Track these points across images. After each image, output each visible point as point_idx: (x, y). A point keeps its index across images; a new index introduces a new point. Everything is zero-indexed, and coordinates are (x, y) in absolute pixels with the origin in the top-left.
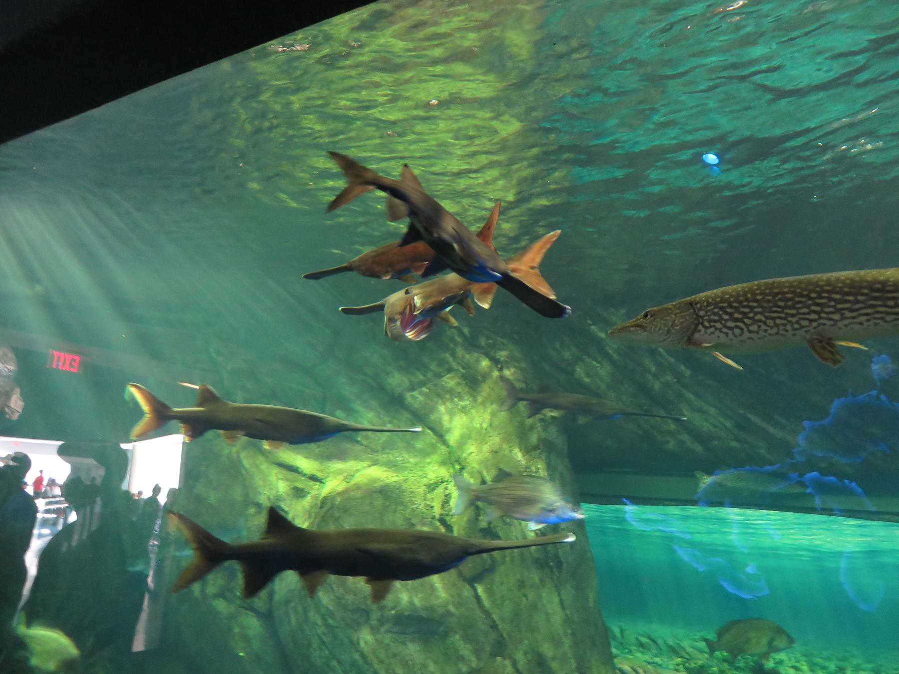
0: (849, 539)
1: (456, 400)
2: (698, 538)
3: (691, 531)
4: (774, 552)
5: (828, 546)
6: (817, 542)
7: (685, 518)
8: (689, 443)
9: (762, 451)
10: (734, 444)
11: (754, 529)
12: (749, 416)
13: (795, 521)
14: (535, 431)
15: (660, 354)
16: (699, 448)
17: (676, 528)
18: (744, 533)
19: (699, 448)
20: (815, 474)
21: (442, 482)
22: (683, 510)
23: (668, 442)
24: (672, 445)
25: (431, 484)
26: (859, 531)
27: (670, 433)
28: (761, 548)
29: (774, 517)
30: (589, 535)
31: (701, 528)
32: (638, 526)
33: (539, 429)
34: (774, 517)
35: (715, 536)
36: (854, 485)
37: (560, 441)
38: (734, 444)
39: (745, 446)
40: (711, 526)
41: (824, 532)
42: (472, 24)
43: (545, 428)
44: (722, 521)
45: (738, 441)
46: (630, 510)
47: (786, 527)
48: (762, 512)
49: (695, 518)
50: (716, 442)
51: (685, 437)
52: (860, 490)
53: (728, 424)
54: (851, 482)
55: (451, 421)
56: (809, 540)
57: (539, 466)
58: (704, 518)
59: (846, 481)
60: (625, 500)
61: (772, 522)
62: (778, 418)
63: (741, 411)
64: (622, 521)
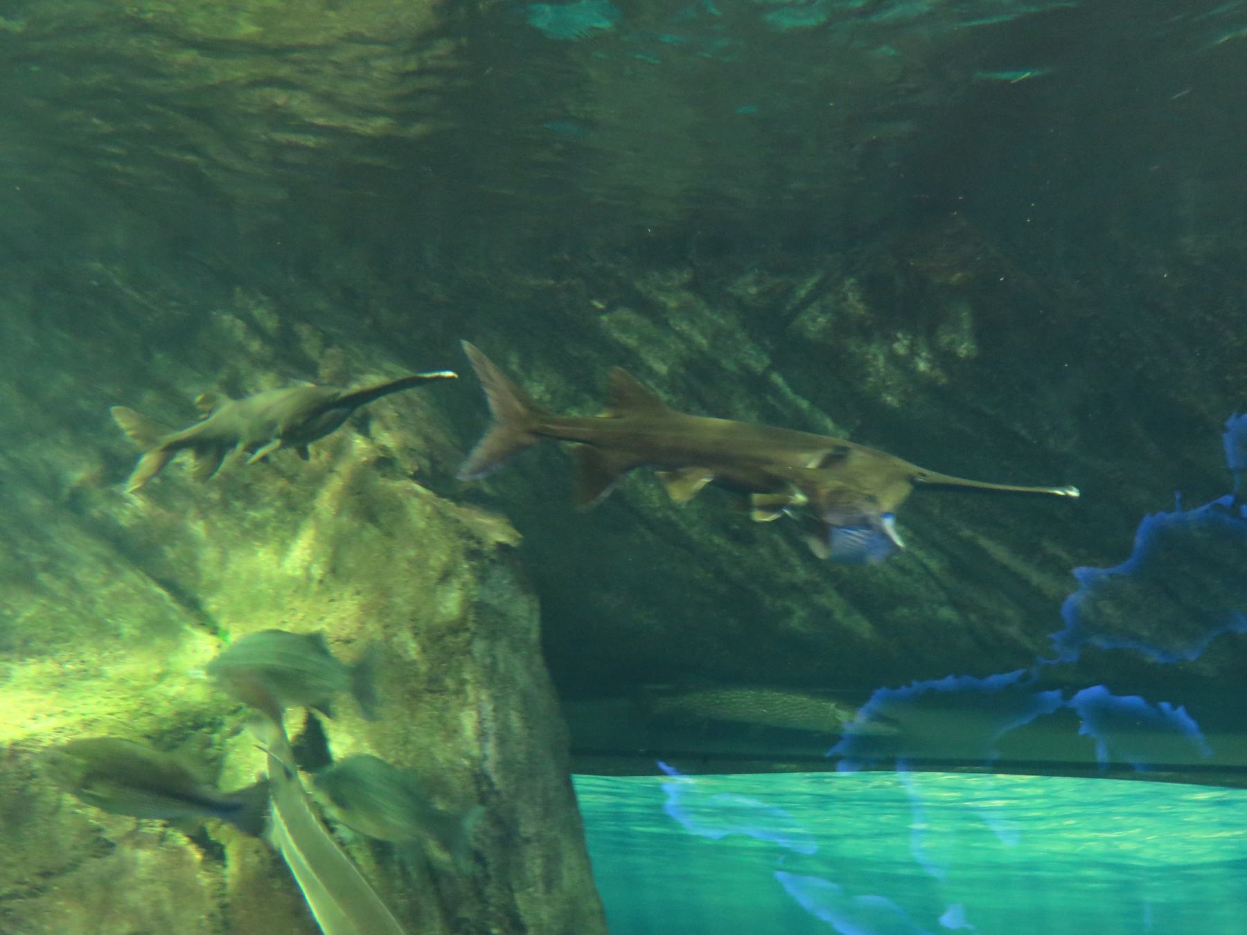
0: (1196, 835)
1: (238, 505)
2: (849, 848)
3: (835, 831)
4: (1031, 876)
5: (1149, 853)
6: (1127, 846)
7: (823, 801)
8: (838, 615)
9: (1013, 631)
10: (947, 613)
11: (981, 820)
12: (984, 542)
13: (1078, 797)
14: (456, 583)
15: (775, 391)
16: (863, 627)
17: (800, 827)
18: (962, 832)
19: (863, 627)
20: (1097, 691)
21: (197, 726)
22: (819, 781)
23: (788, 613)
24: (798, 620)
25: (162, 733)
26: (1217, 814)
27: (793, 588)
28: (999, 866)
29: (1029, 791)
30: (592, 854)
31: (860, 825)
32: (695, 827)
33: (467, 577)
34: (1029, 791)
35: (891, 841)
36: (1181, 712)
37: (524, 611)
38: (947, 613)
39: (973, 617)
40: (882, 819)
41: (1143, 821)
42: (296, 55)
43: (482, 577)
44: (904, 804)
45: (956, 605)
46: (680, 787)
47: (1054, 813)
48: (1002, 778)
49: (845, 800)
50: (905, 611)
51: (830, 600)
52: (1191, 723)
53: (934, 565)
54: (1175, 707)
55: (223, 563)
56: (1108, 841)
57: (467, 676)
58: (867, 799)
59: (1165, 706)
60: (662, 765)
61: (1025, 803)
62: (1051, 548)
63: (967, 533)
64: (659, 815)
